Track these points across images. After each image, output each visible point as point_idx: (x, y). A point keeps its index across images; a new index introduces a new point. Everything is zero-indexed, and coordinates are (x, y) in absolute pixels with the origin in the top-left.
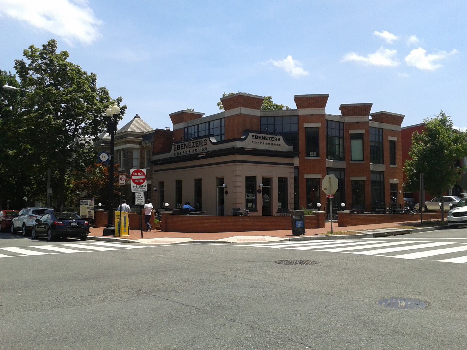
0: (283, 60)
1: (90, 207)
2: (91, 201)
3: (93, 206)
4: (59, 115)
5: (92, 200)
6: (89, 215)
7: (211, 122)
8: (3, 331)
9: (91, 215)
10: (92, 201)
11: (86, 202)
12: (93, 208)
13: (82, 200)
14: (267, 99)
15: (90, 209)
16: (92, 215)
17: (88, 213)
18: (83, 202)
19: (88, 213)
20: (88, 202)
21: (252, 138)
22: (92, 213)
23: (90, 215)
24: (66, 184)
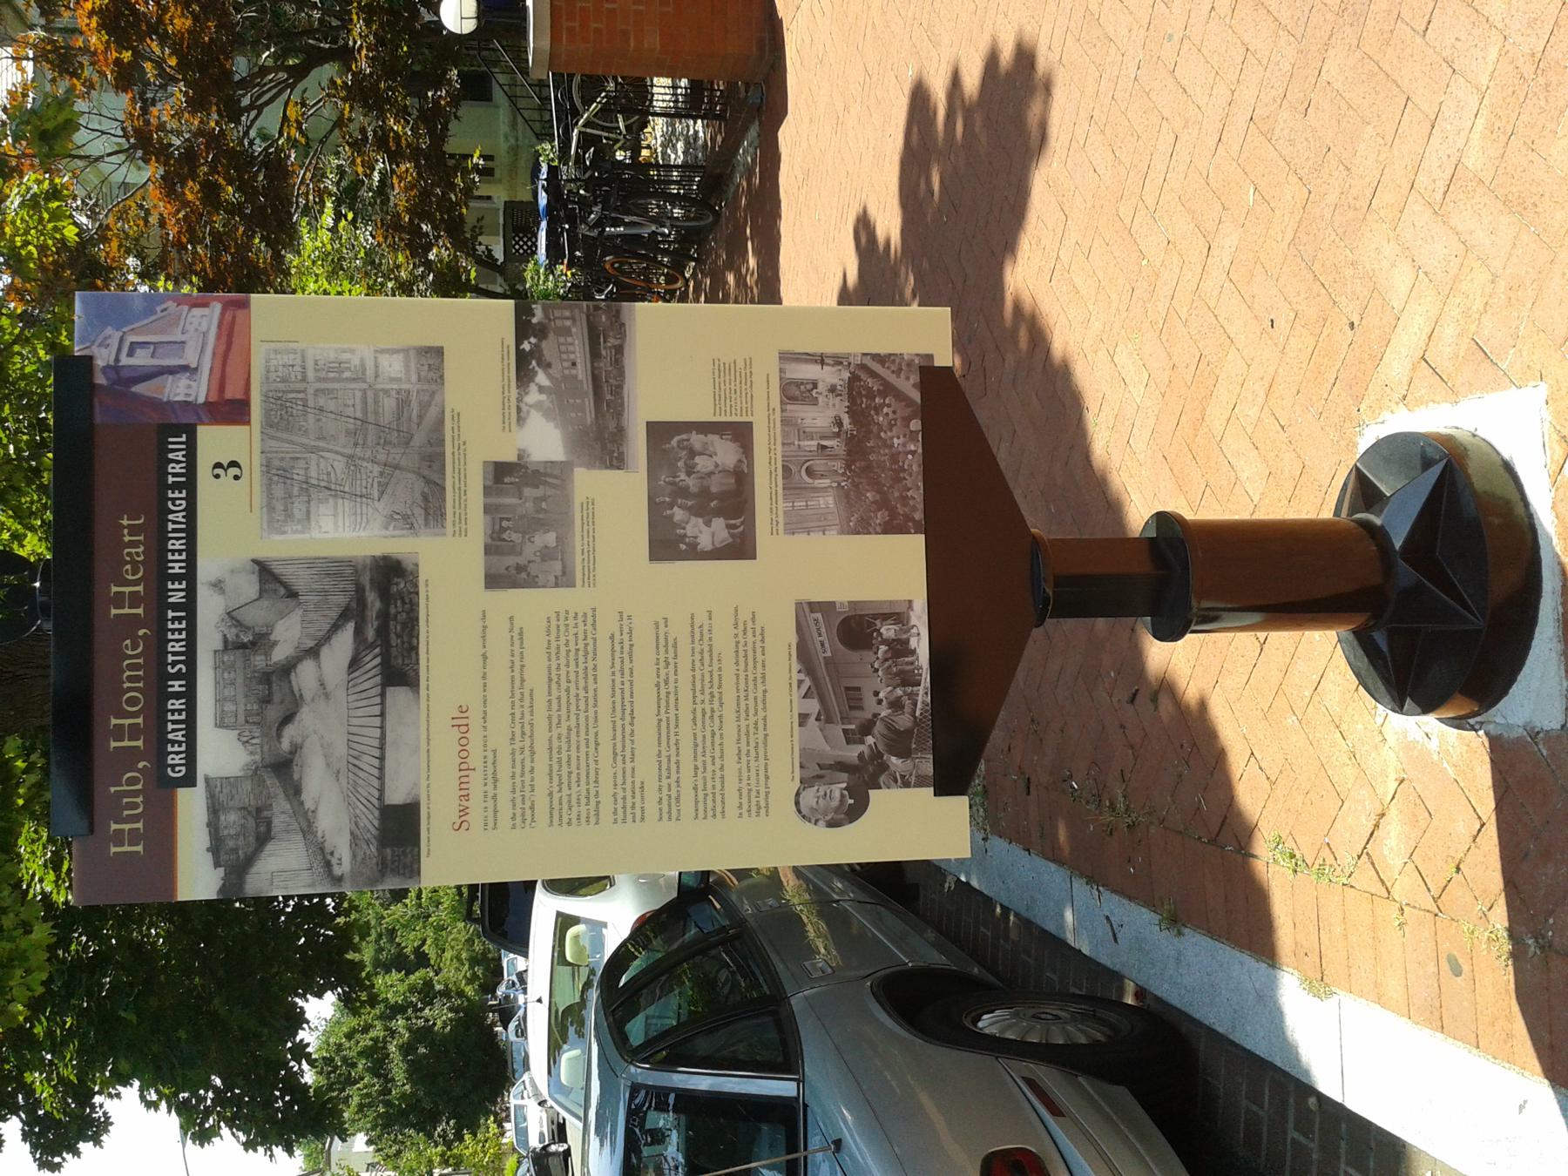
0: (275, 643)
1: (502, 474)
2: (214, 441)
3: (433, 357)
4: (1007, 325)
5: (197, 390)
6: (796, 525)
7: (255, 597)
8: (724, 984)
9: (821, 416)
10: (232, 411)
11: (288, 634)
12: (524, 366)
13: (191, 807)
14: (73, 87)
15: (589, 483)
16: (795, 393)
17: (741, 548)
18: (283, 768)
19: (741, 548)
20: (285, 546)
21: (369, 1165)
22: (728, 374)
23: (793, 478)
24: (699, 121)
